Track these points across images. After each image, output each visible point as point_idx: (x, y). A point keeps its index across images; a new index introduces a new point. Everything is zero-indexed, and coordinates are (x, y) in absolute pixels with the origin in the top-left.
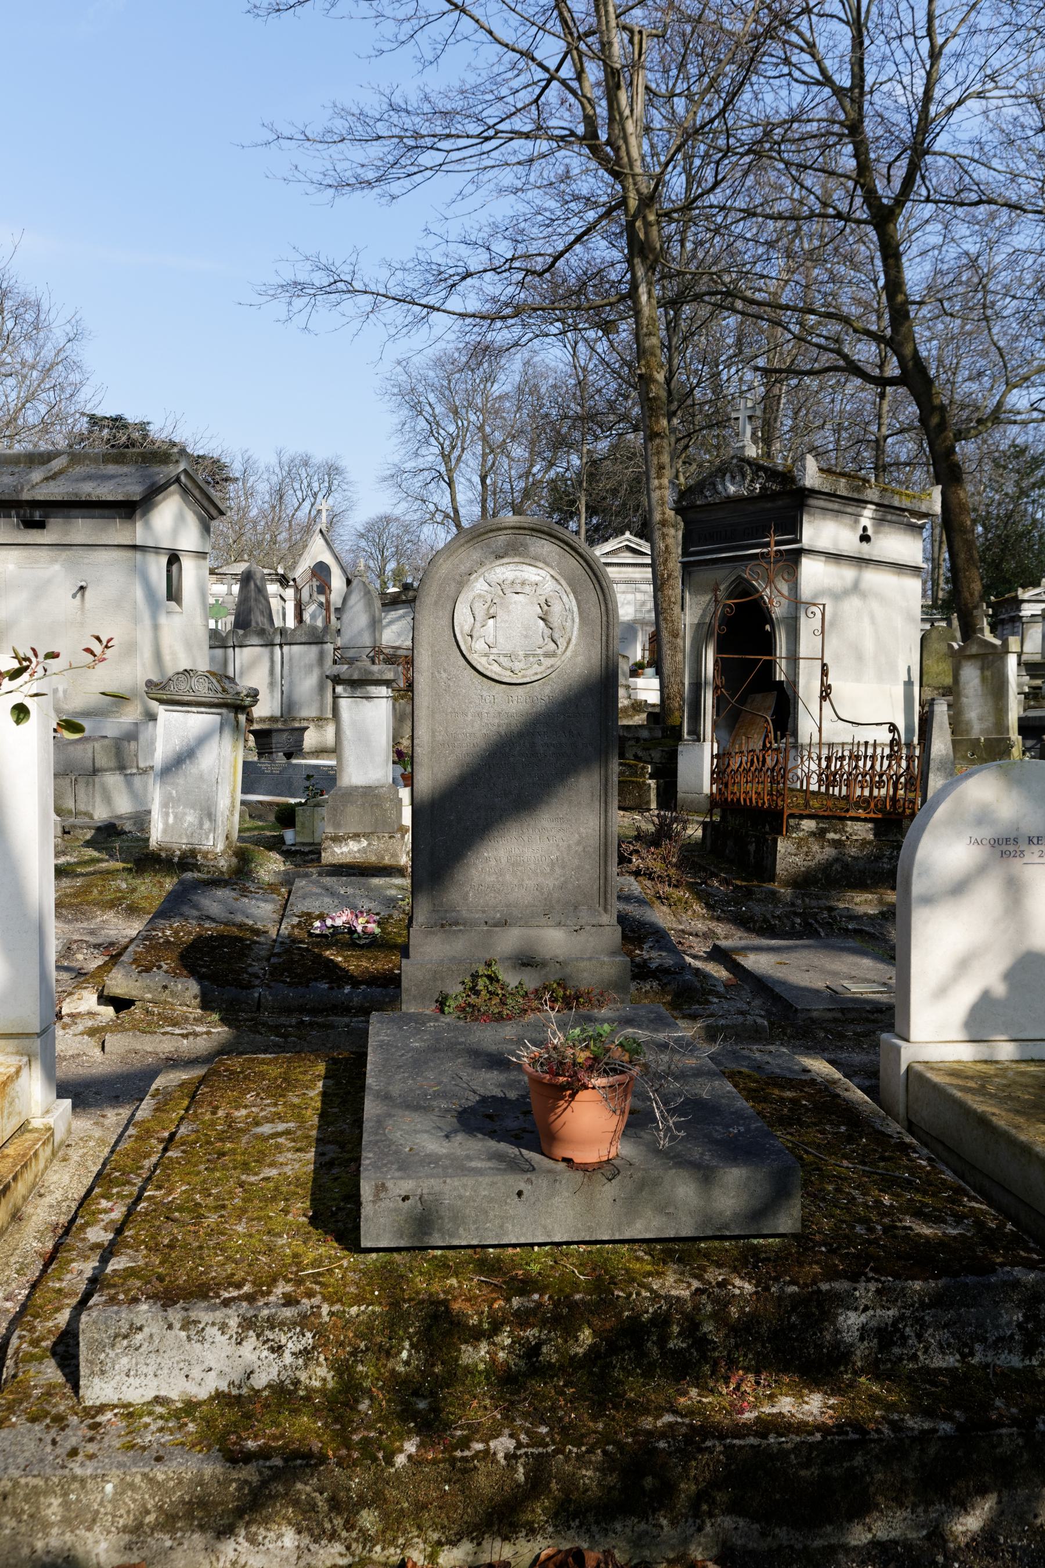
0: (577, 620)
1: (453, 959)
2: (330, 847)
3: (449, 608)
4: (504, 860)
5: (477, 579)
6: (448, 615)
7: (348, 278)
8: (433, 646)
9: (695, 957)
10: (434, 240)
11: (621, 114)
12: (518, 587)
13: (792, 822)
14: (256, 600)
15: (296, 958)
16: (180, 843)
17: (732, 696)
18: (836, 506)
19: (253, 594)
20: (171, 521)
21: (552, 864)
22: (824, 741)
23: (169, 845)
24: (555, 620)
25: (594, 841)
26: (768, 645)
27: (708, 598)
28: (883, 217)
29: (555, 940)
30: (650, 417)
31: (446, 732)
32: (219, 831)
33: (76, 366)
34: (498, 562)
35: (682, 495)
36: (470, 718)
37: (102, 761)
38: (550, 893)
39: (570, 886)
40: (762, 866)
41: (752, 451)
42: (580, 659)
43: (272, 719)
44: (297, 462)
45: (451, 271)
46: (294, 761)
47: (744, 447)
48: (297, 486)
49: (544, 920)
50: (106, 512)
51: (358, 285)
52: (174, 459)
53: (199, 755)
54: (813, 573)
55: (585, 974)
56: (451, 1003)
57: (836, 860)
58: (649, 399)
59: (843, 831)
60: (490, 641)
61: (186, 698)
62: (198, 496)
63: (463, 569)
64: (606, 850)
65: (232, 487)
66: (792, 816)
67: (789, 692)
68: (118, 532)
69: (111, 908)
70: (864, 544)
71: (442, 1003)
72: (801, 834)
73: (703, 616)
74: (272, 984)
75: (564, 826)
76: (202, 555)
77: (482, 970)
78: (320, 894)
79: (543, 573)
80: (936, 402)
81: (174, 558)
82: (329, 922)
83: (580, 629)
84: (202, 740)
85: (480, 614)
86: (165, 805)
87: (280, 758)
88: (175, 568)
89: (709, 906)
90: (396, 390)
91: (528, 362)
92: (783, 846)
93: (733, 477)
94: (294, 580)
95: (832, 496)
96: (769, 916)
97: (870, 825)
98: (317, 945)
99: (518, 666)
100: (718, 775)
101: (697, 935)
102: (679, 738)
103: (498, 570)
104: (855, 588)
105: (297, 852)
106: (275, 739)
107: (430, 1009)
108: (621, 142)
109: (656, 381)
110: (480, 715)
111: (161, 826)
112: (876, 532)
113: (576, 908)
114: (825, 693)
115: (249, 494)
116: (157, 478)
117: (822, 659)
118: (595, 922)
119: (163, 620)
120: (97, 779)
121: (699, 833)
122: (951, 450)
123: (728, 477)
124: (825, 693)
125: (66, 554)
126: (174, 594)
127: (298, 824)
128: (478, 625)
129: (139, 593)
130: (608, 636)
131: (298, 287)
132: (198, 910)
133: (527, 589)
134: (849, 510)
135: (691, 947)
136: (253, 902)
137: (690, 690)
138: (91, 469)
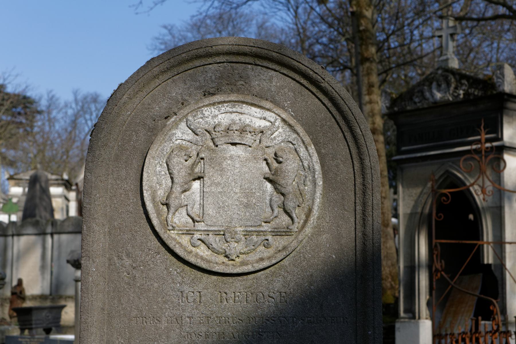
0: (320, 182)
3: (136, 164)
5: (176, 125)
6: (134, 175)
17: (452, 278)
19: (38, 193)
24: (290, 183)
26: (476, 231)
27: (419, 190)
30: (361, 45)
34: (207, 101)
35: (394, 102)
36: (164, 324)
41: (455, 64)
42: (325, 237)
43: (42, 297)
46: (53, 337)
47: (447, 60)
48: (88, 117)
58: (360, 31)
60: (196, 211)
63: (157, 109)
65: (38, 117)
67: (497, 274)
73: (415, 206)
83: (324, 195)
85: (181, 173)
87: (40, 334)
94: (77, 184)
99: (235, 247)
102: (396, 315)
103: (207, 111)
106: (35, 317)
109: (365, 17)
110: (179, 319)
115: (51, 121)
123: (434, 85)
128: (177, 189)
130: (364, 204)
133: (248, 139)
137: (405, 272)
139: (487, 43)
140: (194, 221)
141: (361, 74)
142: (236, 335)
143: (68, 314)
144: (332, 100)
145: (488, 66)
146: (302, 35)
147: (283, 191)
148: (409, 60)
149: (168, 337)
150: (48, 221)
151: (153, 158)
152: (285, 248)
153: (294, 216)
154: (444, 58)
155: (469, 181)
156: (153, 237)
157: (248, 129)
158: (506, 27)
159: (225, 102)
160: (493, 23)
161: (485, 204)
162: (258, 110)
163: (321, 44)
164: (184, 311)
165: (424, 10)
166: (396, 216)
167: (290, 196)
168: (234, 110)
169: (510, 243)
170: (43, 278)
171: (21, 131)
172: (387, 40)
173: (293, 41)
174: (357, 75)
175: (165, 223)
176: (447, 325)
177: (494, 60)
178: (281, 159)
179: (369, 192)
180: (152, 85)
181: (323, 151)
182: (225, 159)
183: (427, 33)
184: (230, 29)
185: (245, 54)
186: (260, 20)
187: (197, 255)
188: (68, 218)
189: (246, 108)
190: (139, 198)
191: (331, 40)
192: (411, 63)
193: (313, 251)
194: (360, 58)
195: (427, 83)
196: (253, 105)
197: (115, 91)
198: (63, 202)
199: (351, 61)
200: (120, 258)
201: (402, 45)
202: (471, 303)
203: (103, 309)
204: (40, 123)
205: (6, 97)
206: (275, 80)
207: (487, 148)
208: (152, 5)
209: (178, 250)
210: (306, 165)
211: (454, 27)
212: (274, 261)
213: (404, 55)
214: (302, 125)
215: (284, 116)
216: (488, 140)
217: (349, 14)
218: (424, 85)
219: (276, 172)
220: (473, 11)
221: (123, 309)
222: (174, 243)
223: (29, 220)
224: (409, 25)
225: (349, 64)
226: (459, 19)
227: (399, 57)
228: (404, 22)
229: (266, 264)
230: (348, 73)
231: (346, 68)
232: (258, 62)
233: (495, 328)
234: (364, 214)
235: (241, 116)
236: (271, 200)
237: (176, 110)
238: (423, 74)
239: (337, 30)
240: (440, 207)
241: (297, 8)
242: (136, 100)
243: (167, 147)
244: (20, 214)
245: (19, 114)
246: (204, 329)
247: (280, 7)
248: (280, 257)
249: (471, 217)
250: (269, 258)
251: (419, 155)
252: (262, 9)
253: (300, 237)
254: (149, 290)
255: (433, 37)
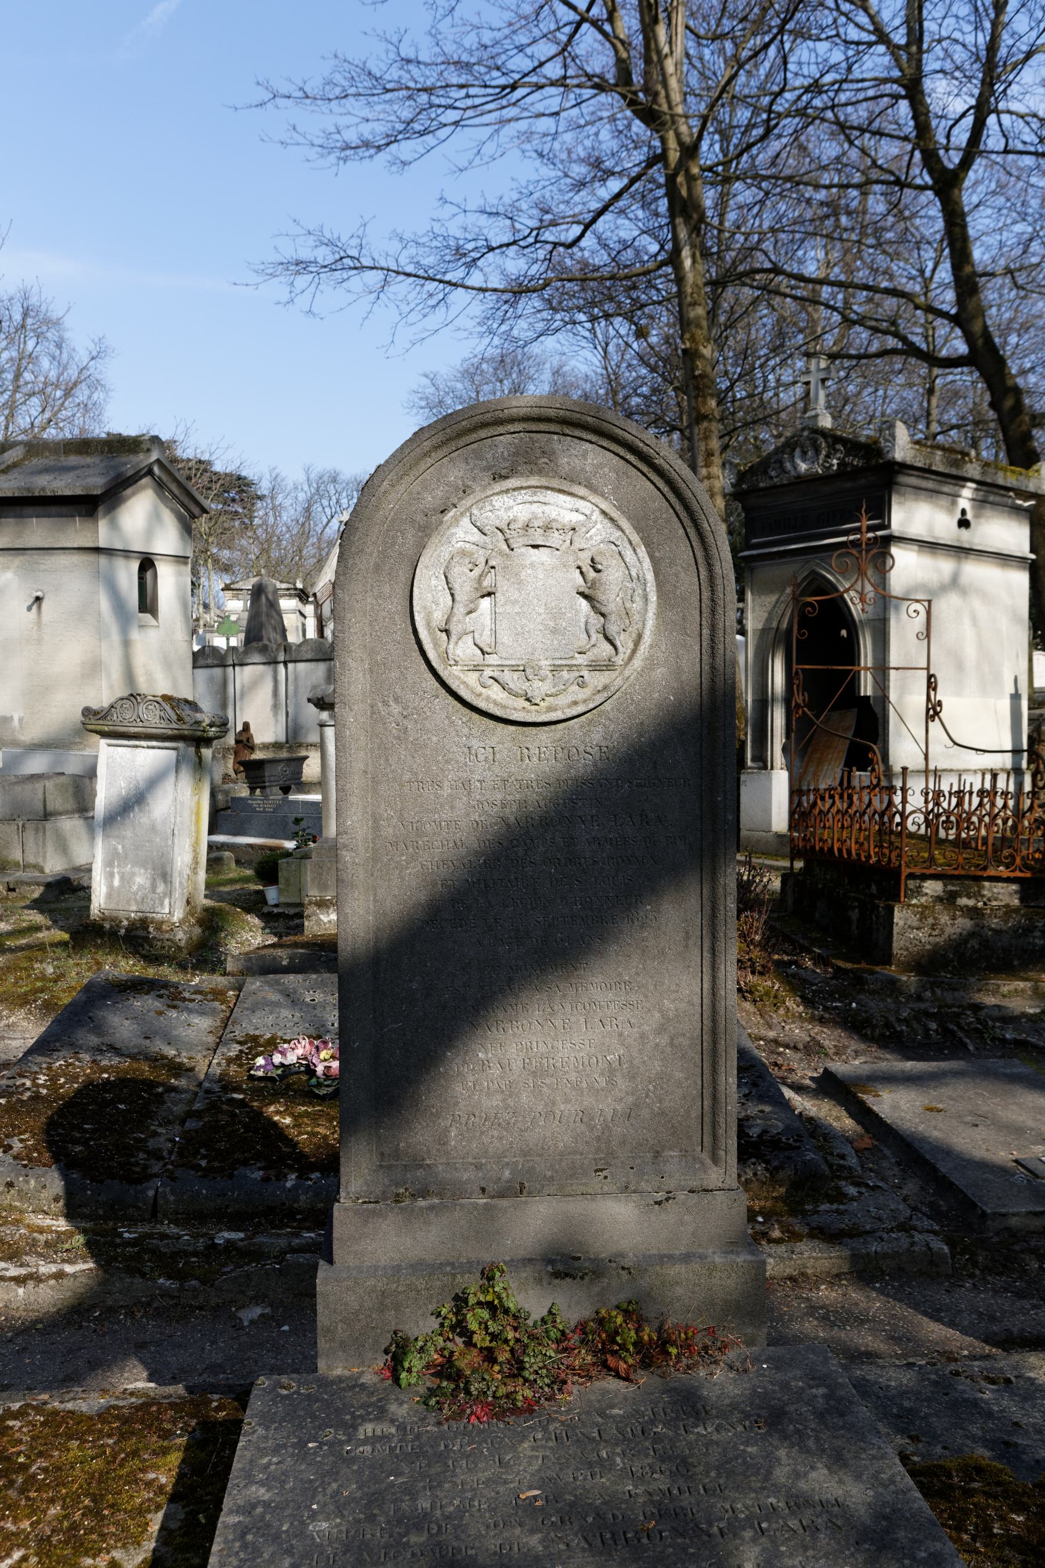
0: (653, 597)
1: (418, 1267)
2: (314, 914)
3: (403, 577)
4: (517, 1065)
5: (456, 520)
6: (401, 591)
7: (354, 253)
8: (372, 653)
9: (798, 1088)
10: (450, 209)
11: (659, 52)
12: (538, 535)
13: (912, 884)
14: (268, 615)
15: (224, 1119)
16: (130, 910)
18: (930, 485)
19: (264, 608)
20: (143, 519)
21: (611, 1072)
22: (932, 767)
23: (114, 914)
25: (691, 1025)
26: (850, 652)
27: (774, 598)
28: (947, 184)
29: (617, 1221)
30: (696, 397)
31: (401, 818)
32: (177, 895)
33: (96, 385)
34: (498, 487)
35: (741, 477)
36: (446, 791)
37: (56, 802)
38: (606, 1127)
39: (645, 1113)
40: (875, 942)
41: (826, 422)
42: (659, 673)
43: (277, 746)
44: (325, 478)
45: (470, 246)
46: (292, 797)
47: (816, 416)
48: (325, 502)
49: (595, 1183)
50: (64, 509)
51: (366, 262)
52: (145, 447)
53: (150, 800)
54: (907, 567)
55: (679, 1291)
56: (415, 1362)
57: (972, 934)
58: (695, 377)
59: (978, 895)
60: (485, 640)
61: (133, 730)
62: (176, 491)
63: (429, 500)
64: (715, 1043)
65: (259, 504)
66: (911, 876)
67: (877, 710)
68: (77, 533)
69: (21, 1006)
70: (963, 530)
71: (397, 1353)
72: (923, 900)
73: (769, 620)
74: (179, 1173)
75: (633, 998)
76: (181, 559)
77: (472, 1284)
78: (277, 1004)
79: (585, 506)
80: (1010, 383)
81: (147, 563)
82: (277, 1059)
83: (659, 615)
84: (154, 782)
85: (464, 588)
86: (109, 863)
87: (276, 794)
88: (149, 575)
89: (807, 1001)
90: (423, 403)
91: (557, 372)
92: (900, 916)
93: (804, 453)
94: (315, 595)
95: (926, 472)
96: (892, 1019)
97: (1014, 887)
98: (257, 1093)
99: (539, 688)
100: (798, 815)
101: (795, 1048)
102: (741, 764)
103: (498, 501)
104: (954, 583)
105: (279, 915)
107: (371, 1371)
108: (659, 87)
109: (702, 356)
110: (466, 784)
111: (104, 889)
112: (977, 516)
113: (657, 1154)
114: (933, 711)
116: (123, 469)
117: (928, 669)
118: (694, 1184)
119: (135, 635)
120: (48, 825)
121: (776, 884)
122: (1028, 437)
123: (798, 452)
124: (933, 711)
125: (18, 560)
126: (147, 604)
127: (281, 880)
128: (460, 609)
129: (104, 604)
130: (713, 627)
131: (301, 266)
132: (100, 1034)
133: (555, 539)
134: (946, 489)
135: (791, 1070)
136: (184, 1016)
137: (754, 708)
138: (50, 461)
139: (870, 390)
140: (483, 652)
141: (696, 438)
142: (542, 804)
143: (311, 769)
144: (669, 482)
145: (869, 423)
146: (613, 382)
147: (603, 610)
148: (761, 416)
149: (452, 807)
150: (279, 645)
151: (427, 567)
152: (606, 688)
153: (618, 644)
154: (813, 413)
155: (843, 585)
156: (429, 675)
157: (554, 525)
158: (898, 366)
159: (522, 488)
160: (878, 361)
161: (863, 616)
162: (568, 498)
163: (639, 395)
164: (472, 772)
165: (782, 345)
166: (742, 632)
167: (613, 618)
168: (535, 499)
169: (897, 669)
170: (277, 721)
171: (237, 523)
172: (731, 388)
173: (602, 392)
174: (690, 439)
175: (445, 656)
176: (809, 777)
177: (877, 414)
178: (599, 567)
179: (720, 611)
180: (423, 466)
181: (657, 554)
182: (524, 567)
183: (787, 377)
184: (514, 376)
185: (548, 420)
186: (555, 364)
187: (488, 699)
188: (306, 641)
189: (551, 496)
190: (409, 622)
191: (654, 391)
192: (764, 421)
193: (644, 690)
194: (694, 415)
195: (788, 450)
196: (560, 491)
197: (372, 476)
198: (297, 621)
199: (681, 420)
200: (386, 704)
201: (750, 396)
202: (841, 749)
203: (365, 772)
204: (261, 513)
205: (214, 478)
206: (589, 456)
207: (869, 539)
208: (409, 345)
209: (463, 693)
210: (634, 574)
211: (828, 369)
212: (591, 706)
213: (754, 410)
214: (629, 519)
215: (604, 506)
216: (871, 529)
217: (680, 352)
218: (783, 452)
219: (593, 585)
220: (850, 344)
221: (393, 771)
222: (457, 683)
223: (254, 644)
224: (761, 366)
225: (678, 423)
226: (832, 357)
227: (747, 413)
228: (754, 363)
229: (581, 709)
230: (676, 436)
231: (674, 429)
232: (567, 431)
233: (875, 782)
234: (712, 640)
235: (544, 507)
236: (587, 623)
237: (455, 501)
238: (779, 436)
239: (662, 375)
240: (804, 620)
241: (607, 344)
242: (401, 488)
243: (445, 552)
244: (242, 636)
245: (233, 500)
246: (499, 796)
247: (584, 343)
248: (599, 699)
249: (844, 633)
250: (585, 701)
251: (775, 549)
252: (558, 346)
253: (627, 673)
254: (426, 745)
255: (795, 383)
